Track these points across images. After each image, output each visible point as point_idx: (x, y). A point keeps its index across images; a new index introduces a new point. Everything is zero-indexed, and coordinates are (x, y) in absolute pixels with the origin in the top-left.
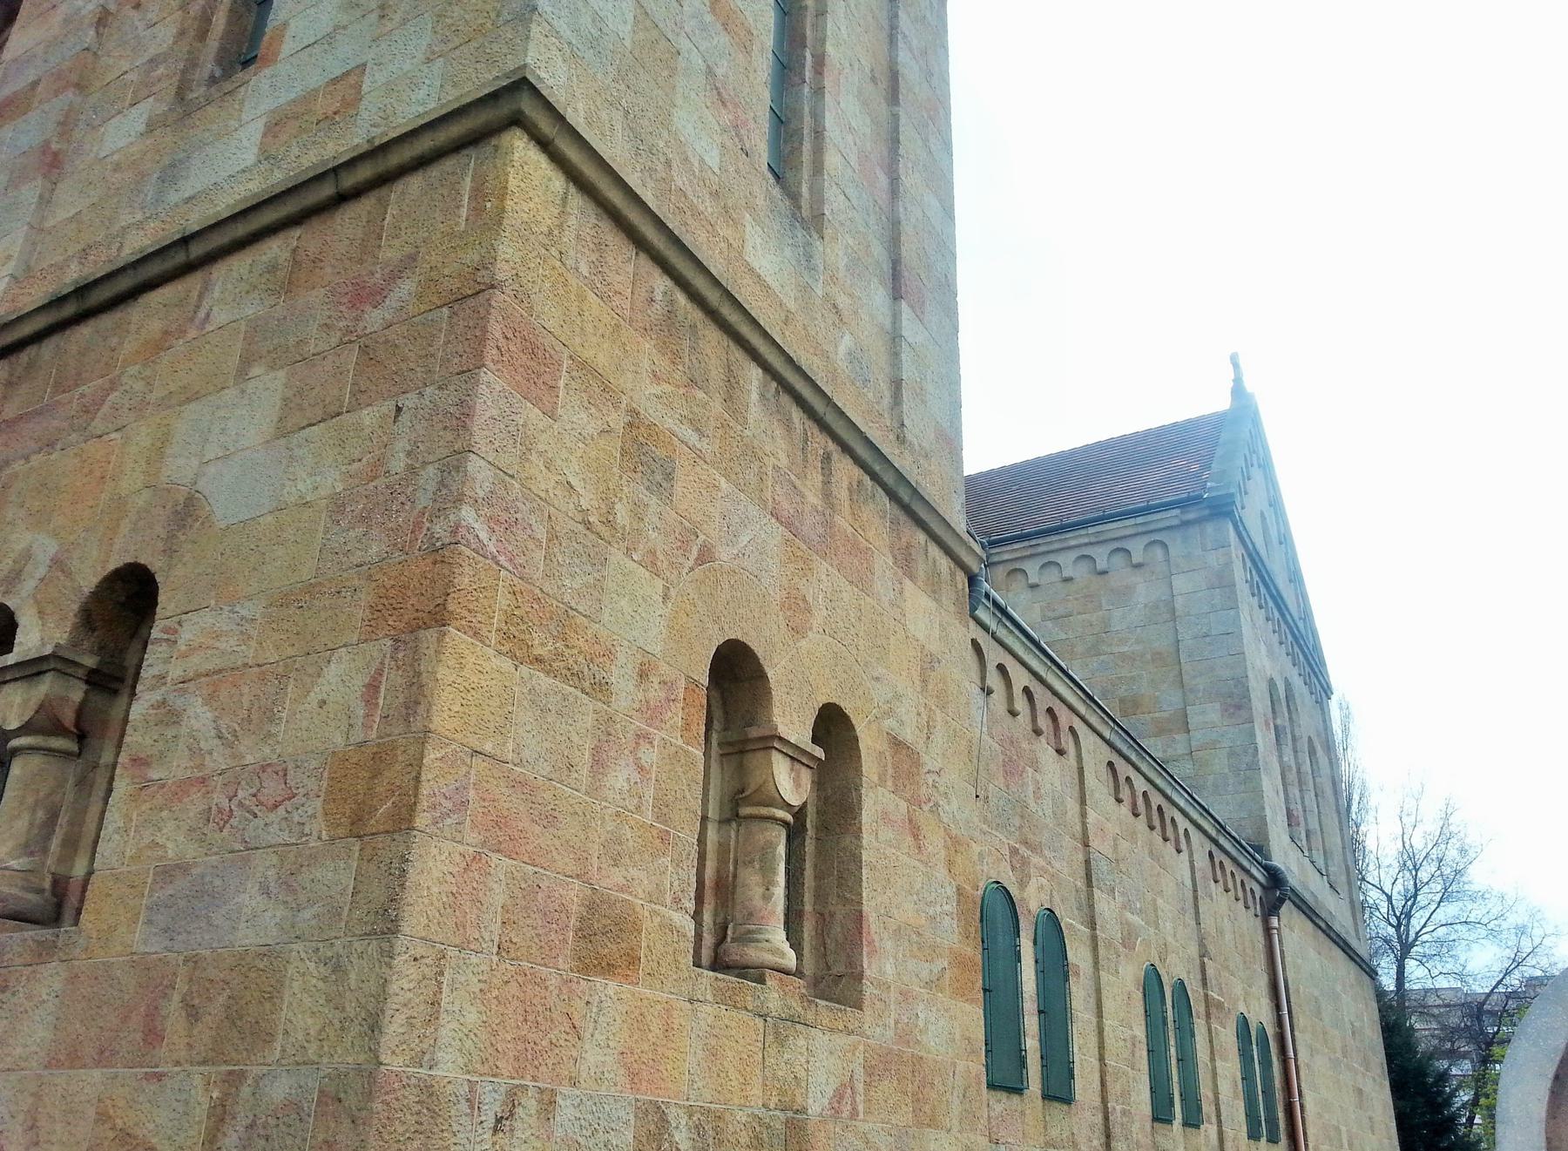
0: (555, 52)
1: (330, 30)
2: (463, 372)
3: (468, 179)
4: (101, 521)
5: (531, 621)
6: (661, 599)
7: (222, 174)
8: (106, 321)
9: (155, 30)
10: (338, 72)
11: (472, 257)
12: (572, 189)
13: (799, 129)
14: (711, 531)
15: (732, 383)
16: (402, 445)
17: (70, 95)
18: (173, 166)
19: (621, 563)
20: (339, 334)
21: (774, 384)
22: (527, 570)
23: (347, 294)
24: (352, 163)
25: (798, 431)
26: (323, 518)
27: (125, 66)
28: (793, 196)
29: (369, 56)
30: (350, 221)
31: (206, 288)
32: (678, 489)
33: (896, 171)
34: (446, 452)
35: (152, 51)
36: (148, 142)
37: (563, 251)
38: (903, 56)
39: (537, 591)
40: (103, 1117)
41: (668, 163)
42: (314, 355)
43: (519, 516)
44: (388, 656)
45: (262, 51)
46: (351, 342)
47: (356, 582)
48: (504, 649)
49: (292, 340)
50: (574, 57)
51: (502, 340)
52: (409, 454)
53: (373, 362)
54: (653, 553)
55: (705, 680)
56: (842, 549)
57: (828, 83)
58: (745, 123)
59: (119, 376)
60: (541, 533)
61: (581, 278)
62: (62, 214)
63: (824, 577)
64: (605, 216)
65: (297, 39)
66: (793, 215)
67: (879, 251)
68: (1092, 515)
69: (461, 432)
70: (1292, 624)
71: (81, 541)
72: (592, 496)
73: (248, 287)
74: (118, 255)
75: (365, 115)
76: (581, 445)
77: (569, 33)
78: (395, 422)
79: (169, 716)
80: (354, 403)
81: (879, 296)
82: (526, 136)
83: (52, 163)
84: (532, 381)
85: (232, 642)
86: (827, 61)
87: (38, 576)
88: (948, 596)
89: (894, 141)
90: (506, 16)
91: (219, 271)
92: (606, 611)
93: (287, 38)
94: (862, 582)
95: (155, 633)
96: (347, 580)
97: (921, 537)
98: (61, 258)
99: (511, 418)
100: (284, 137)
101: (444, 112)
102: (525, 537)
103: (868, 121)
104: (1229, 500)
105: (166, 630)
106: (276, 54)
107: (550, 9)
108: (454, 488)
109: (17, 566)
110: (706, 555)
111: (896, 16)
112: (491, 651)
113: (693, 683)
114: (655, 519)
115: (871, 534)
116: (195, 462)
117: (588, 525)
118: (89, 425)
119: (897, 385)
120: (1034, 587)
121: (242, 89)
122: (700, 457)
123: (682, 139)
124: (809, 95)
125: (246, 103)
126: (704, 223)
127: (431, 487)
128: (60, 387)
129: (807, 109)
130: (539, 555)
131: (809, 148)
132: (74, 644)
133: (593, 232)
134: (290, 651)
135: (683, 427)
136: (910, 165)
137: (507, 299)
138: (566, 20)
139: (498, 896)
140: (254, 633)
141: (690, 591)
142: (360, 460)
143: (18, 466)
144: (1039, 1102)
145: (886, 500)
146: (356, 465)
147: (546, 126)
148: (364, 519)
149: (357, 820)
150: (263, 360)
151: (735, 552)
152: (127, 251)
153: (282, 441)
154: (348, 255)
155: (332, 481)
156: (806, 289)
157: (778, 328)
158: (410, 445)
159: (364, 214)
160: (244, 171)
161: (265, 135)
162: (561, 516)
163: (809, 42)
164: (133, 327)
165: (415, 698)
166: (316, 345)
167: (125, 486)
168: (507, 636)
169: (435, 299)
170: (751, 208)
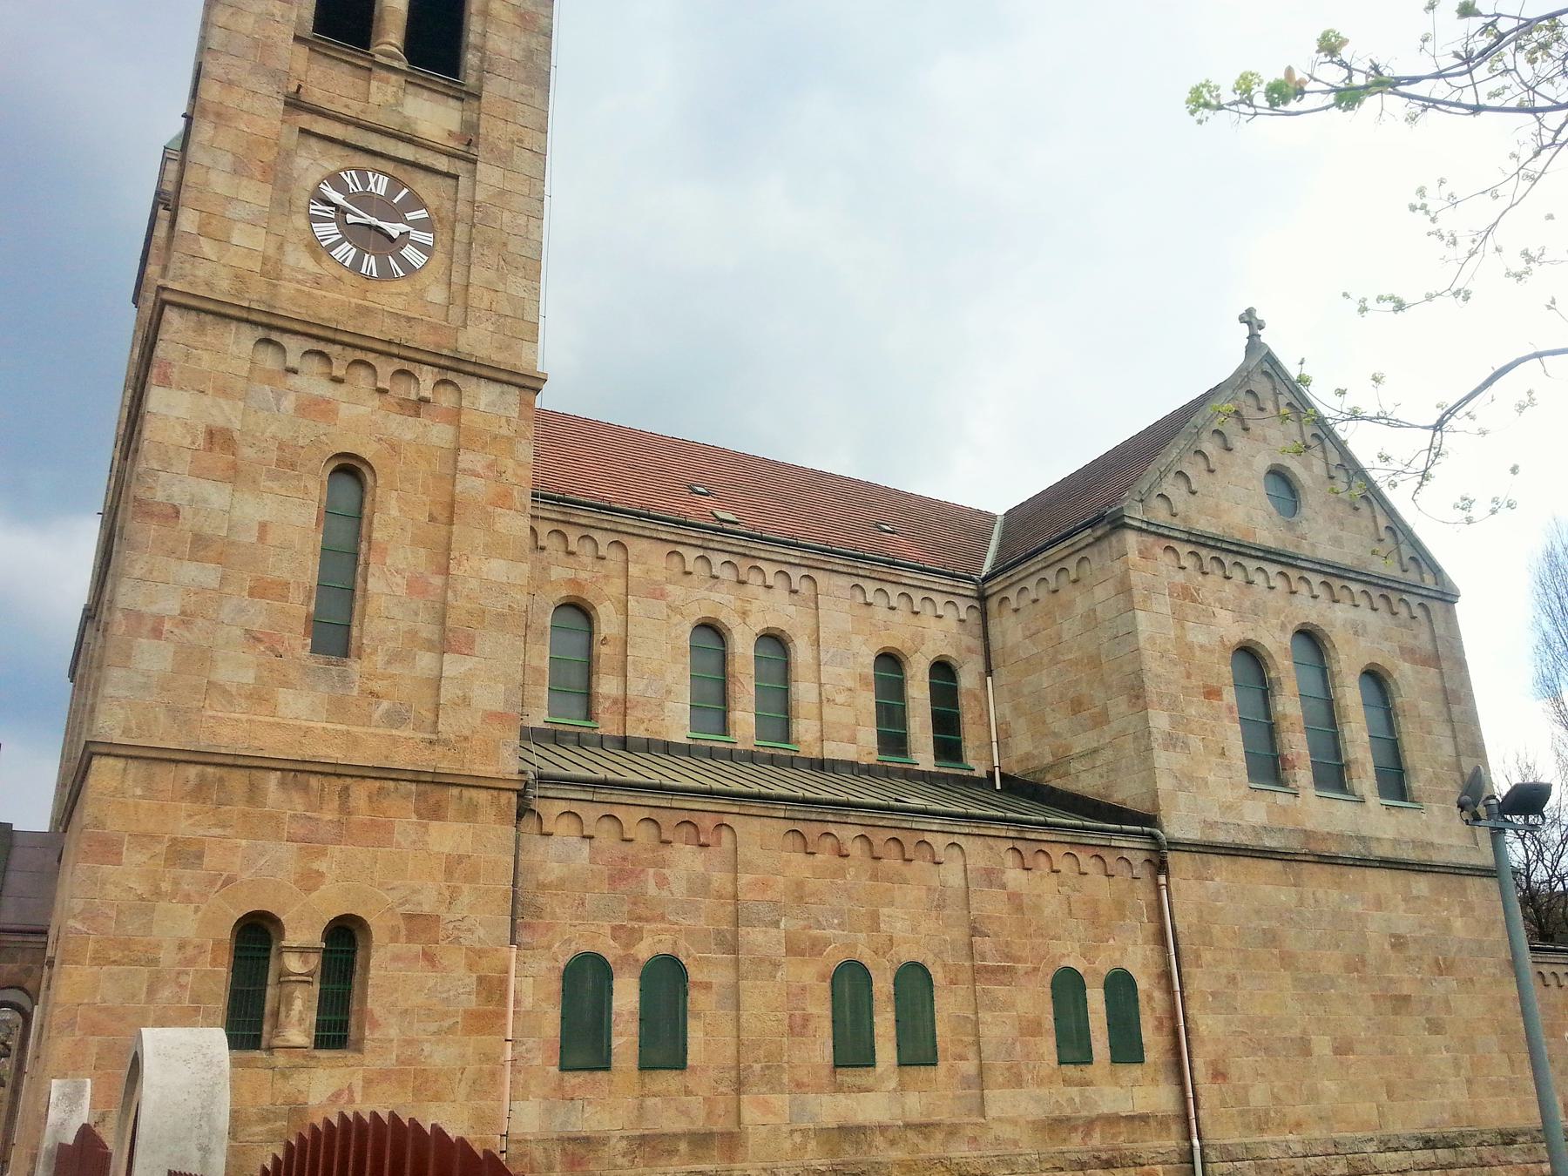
68: (582, 499)
88: (488, 814)
104: (1120, 514)
120: (1016, 610)
144: (636, 1073)
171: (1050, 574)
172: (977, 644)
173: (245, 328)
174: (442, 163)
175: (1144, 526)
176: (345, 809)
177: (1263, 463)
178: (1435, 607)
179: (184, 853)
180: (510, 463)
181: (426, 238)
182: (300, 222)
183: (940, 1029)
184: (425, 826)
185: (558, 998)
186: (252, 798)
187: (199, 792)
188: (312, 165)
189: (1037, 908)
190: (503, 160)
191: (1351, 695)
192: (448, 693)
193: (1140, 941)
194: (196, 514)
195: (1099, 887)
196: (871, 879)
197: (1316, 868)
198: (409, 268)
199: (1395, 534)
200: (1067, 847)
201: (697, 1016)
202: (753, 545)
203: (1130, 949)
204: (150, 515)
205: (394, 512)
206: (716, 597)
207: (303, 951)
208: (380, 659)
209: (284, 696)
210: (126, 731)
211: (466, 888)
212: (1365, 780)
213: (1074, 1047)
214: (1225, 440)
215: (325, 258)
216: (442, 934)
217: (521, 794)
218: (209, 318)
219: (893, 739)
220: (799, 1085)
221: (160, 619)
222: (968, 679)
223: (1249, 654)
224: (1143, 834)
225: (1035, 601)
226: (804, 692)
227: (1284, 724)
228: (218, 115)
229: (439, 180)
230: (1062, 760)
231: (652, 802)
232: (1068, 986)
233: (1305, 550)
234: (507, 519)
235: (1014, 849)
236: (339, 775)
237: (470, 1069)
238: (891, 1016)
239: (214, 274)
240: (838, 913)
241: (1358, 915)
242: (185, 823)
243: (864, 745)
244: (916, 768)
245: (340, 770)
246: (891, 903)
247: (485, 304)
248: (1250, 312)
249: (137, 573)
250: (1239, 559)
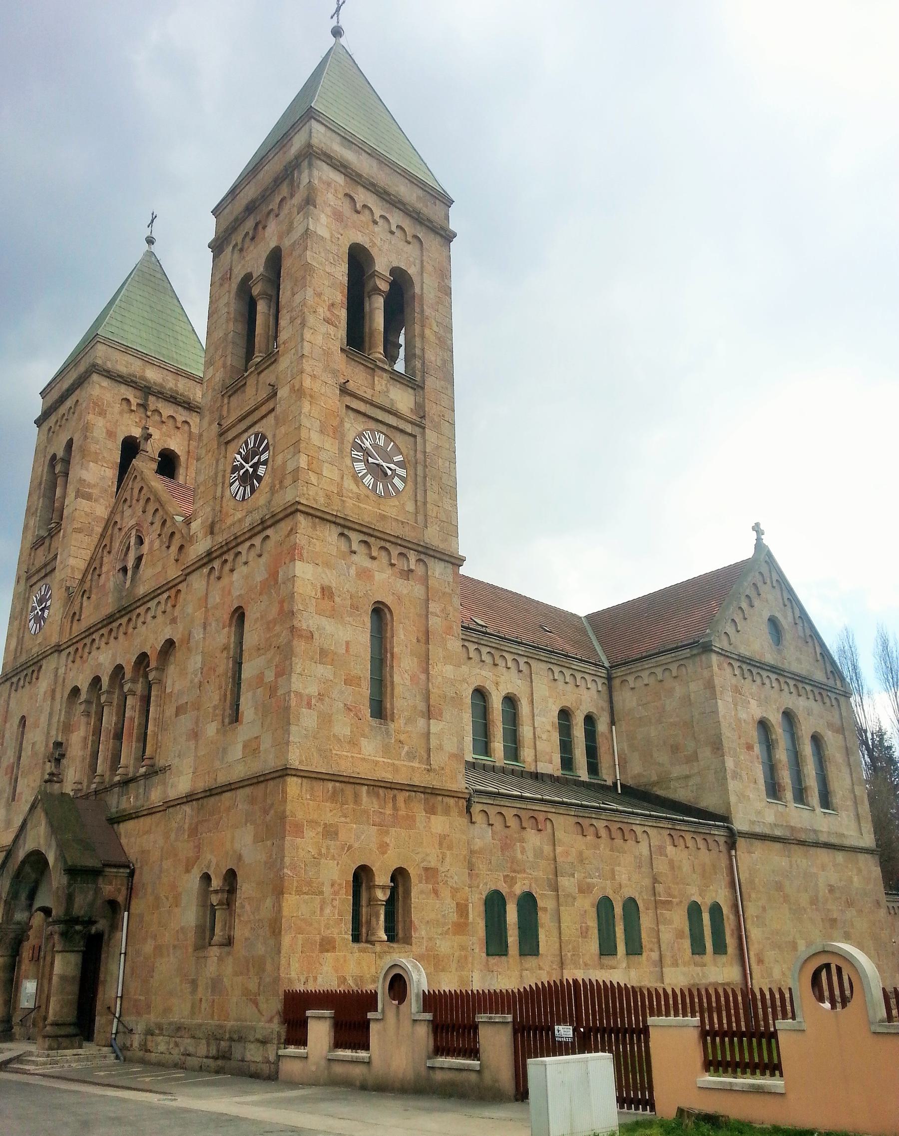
40: (243, 985)
70: (793, 676)
79: (243, 907)
88: (454, 812)
110: (350, 847)
113: (347, 882)
120: (632, 689)
139: (300, 942)
144: (518, 957)
149: (274, 932)
165: (280, 910)
171: (659, 671)
172: (606, 705)
173: (333, 526)
174: (409, 428)
175: (720, 651)
176: (395, 808)
177: (766, 615)
178: (842, 700)
179: (330, 832)
180: (451, 608)
181: (402, 472)
182: (348, 461)
183: (644, 935)
184: (429, 818)
185: (483, 915)
186: (356, 801)
187: (333, 797)
188: (353, 427)
189: (680, 868)
190: (437, 428)
191: (807, 749)
192: (434, 742)
193: (723, 887)
194: (320, 637)
195: (705, 856)
196: (610, 851)
197: (796, 847)
198: (398, 491)
199: (823, 656)
200: (692, 834)
201: (542, 927)
202: (502, 643)
203: (719, 891)
204: (301, 636)
205: (402, 637)
206: (484, 673)
207: (383, 888)
208: (402, 721)
209: (364, 742)
210: (301, 762)
211: (448, 853)
212: (814, 798)
213: (698, 948)
214: (751, 601)
215: (360, 484)
216: (440, 879)
217: (469, 801)
218: (317, 520)
219: (567, 763)
220: (586, 965)
221: (310, 698)
222: (602, 726)
223: (763, 725)
224: (723, 827)
225: (646, 685)
226: (526, 731)
227: (780, 766)
228: (311, 396)
229: (407, 437)
230: (664, 780)
231: (518, 805)
232: (694, 911)
233: (786, 666)
234: (452, 641)
235: (500, 813)
236: (391, 788)
237: (456, 954)
238: (622, 927)
239: (317, 494)
240: (598, 869)
241: (814, 873)
242: (330, 814)
243: (551, 766)
244: (580, 779)
245: (393, 786)
246: (619, 865)
247: (434, 515)
248: (757, 525)
249: (298, 671)
250: (760, 671)
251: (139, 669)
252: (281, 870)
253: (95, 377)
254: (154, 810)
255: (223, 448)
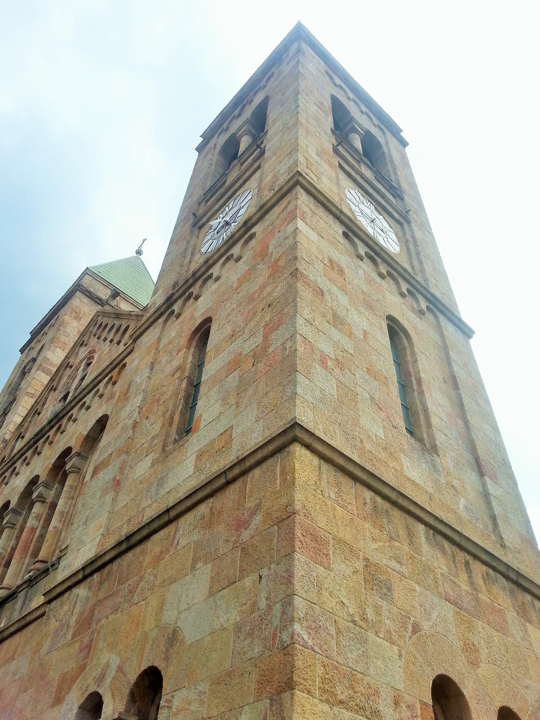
0: (306, 408)
1: (218, 414)
2: (287, 555)
3: (278, 467)
4: (137, 645)
5: (335, 680)
6: (398, 657)
7: (181, 479)
8: (138, 550)
9: (154, 426)
10: (222, 431)
11: (284, 501)
12: (322, 462)
13: (415, 412)
14: (416, 615)
15: (410, 534)
16: (263, 595)
17: (124, 456)
18: (162, 479)
19: (374, 640)
20: (232, 544)
21: (432, 531)
22: (329, 652)
23: (234, 525)
24: (231, 468)
25: (449, 553)
26: (232, 636)
27: (143, 441)
28: (420, 440)
29: (234, 422)
30: (233, 491)
31: (177, 530)
32: (395, 595)
33: (466, 418)
34: (284, 596)
35: (153, 434)
36: (152, 470)
37: (322, 490)
38: (456, 369)
39: (335, 663)
41: (361, 441)
42: (222, 555)
43: (321, 624)
44: (268, 709)
45: (193, 426)
46: (237, 547)
47: (250, 669)
48: (323, 699)
49: (213, 549)
50: (314, 408)
51: (301, 537)
52: (267, 599)
53: (247, 555)
54: (389, 632)
55: (430, 702)
56: (487, 612)
57: (425, 388)
58: (392, 414)
59: (144, 575)
60: (333, 631)
61: (332, 501)
62: (121, 505)
63: (481, 630)
64: (338, 471)
65: (206, 420)
66: (423, 449)
67: (467, 455)
69: (289, 585)
71: (129, 657)
72: (354, 607)
73: (193, 527)
74: (142, 520)
75: (234, 447)
76: (345, 581)
77: (311, 399)
78: (259, 583)
80: (241, 576)
81: (471, 477)
82: (300, 445)
83: (117, 484)
84: (318, 554)
85: (197, 706)
86: (422, 380)
87: (112, 676)
89: (461, 405)
90: (285, 398)
91: (182, 521)
92: (371, 669)
93: (202, 421)
94: (503, 629)
95: (162, 703)
96: (246, 667)
97: (529, 597)
98: (120, 524)
99: (310, 574)
100: (203, 461)
101: (265, 441)
102: (326, 634)
103: (447, 399)
105: (167, 701)
106: (198, 428)
107: (303, 392)
108: (289, 614)
109: (103, 671)
110: (416, 629)
111: (449, 354)
112: (316, 701)
114: (387, 614)
115: (500, 601)
116: (176, 612)
117: (354, 622)
118: (132, 599)
119: (493, 518)
121: (186, 443)
122: (403, 576)
123: (366, 428)
124: (417, 396)
125: (188, 449)
126: (383, 463)
127: (279, 615)
128: (120, 583)
129: (418, 401)
130: (333, 643)
131: (423, 417)
132: (127, 711)
133: (334, 479)
134: (223, 709)
135: (391, 562)
136: (472, 414)
137: (301, 517)
138: (309, 394)
140: (206, 700)
141: (412, 650)
142: (246, 604)
143: (104, 621)
145: (504, 580)
146: (245, 606)
147: (307, 439)
148: (250, 634)
150: (202, 560)
151: (431, 624)
152: (145, 518)
153: (212, 598)
154: (233, 507)
155: (234, 616)
156: (436, 482)
157: (427, 503)
158: (267, 594)
159: (238, 489)
160: (189, 477)
161: (196, 461)
162: (341, 620)
163: (412, 374)
164: (149, 551)
166: (223, 551)
167: (147, 627)
168: (325, 691)
169: (271, 523)
170: (403, 451)
251: (58, 474)
252: (285, 627)
253: (78, 294)
254: (29, 619)
255: (196, 232)
